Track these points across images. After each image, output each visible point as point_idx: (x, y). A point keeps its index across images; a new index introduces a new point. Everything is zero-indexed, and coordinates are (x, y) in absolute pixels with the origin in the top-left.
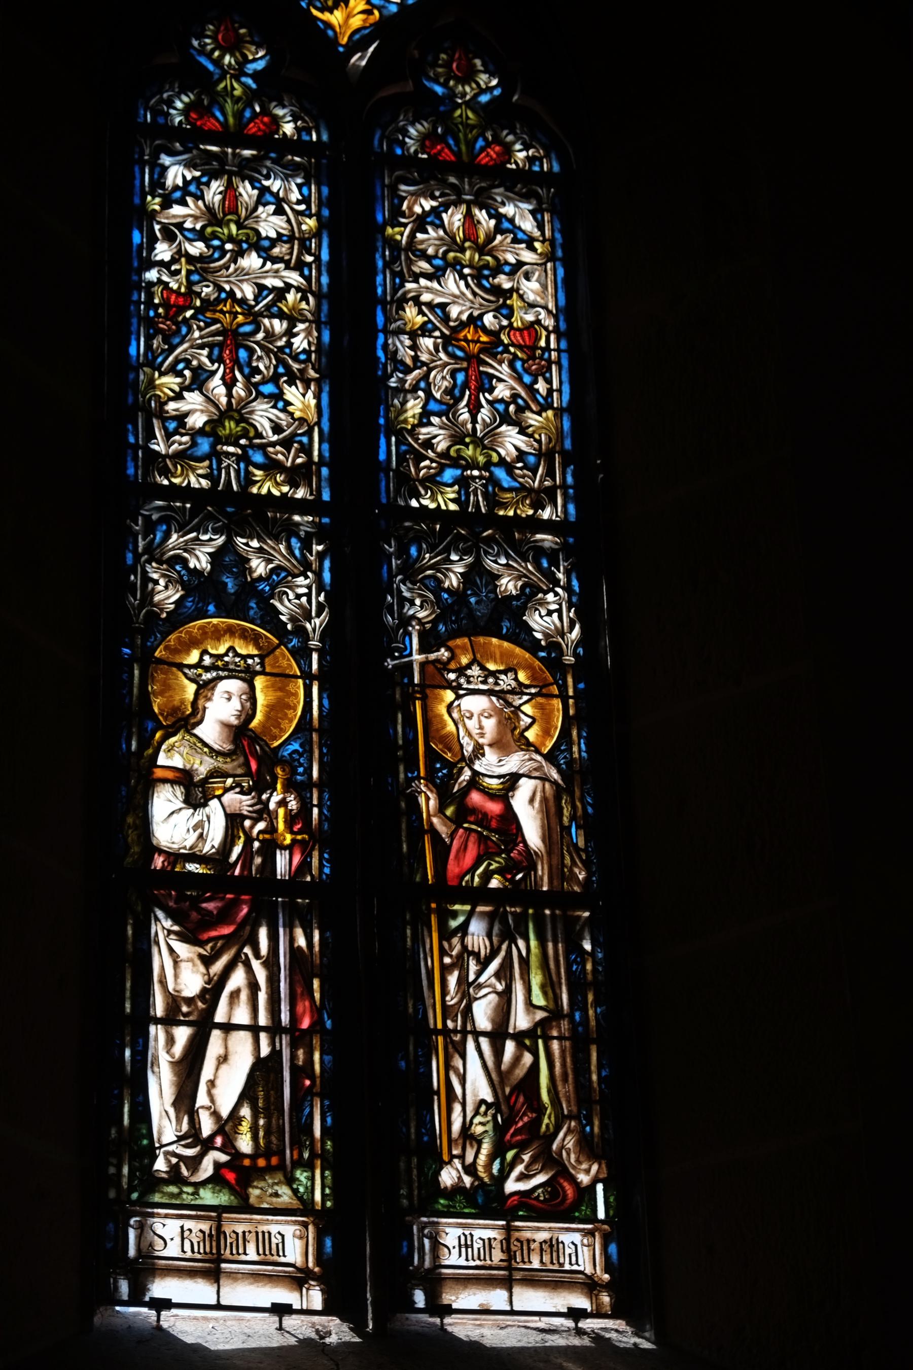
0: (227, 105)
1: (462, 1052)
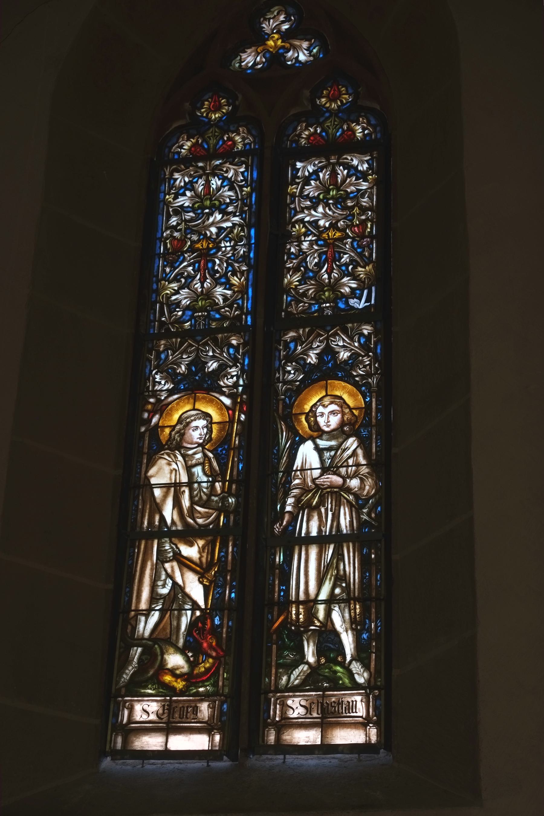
0: (330, 130)
1: (197, 608)
